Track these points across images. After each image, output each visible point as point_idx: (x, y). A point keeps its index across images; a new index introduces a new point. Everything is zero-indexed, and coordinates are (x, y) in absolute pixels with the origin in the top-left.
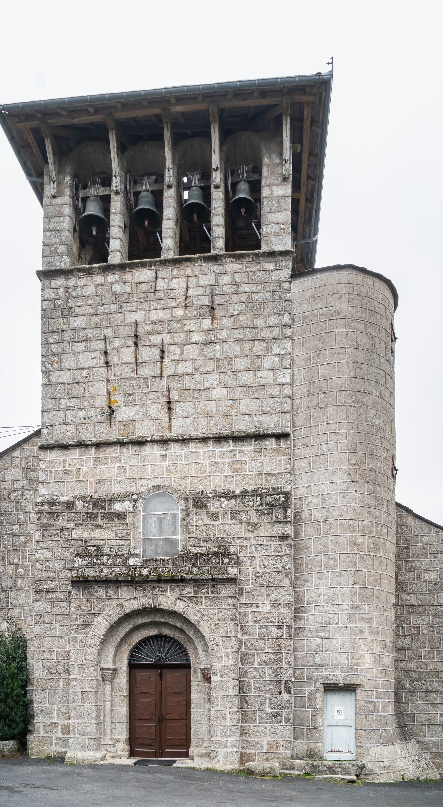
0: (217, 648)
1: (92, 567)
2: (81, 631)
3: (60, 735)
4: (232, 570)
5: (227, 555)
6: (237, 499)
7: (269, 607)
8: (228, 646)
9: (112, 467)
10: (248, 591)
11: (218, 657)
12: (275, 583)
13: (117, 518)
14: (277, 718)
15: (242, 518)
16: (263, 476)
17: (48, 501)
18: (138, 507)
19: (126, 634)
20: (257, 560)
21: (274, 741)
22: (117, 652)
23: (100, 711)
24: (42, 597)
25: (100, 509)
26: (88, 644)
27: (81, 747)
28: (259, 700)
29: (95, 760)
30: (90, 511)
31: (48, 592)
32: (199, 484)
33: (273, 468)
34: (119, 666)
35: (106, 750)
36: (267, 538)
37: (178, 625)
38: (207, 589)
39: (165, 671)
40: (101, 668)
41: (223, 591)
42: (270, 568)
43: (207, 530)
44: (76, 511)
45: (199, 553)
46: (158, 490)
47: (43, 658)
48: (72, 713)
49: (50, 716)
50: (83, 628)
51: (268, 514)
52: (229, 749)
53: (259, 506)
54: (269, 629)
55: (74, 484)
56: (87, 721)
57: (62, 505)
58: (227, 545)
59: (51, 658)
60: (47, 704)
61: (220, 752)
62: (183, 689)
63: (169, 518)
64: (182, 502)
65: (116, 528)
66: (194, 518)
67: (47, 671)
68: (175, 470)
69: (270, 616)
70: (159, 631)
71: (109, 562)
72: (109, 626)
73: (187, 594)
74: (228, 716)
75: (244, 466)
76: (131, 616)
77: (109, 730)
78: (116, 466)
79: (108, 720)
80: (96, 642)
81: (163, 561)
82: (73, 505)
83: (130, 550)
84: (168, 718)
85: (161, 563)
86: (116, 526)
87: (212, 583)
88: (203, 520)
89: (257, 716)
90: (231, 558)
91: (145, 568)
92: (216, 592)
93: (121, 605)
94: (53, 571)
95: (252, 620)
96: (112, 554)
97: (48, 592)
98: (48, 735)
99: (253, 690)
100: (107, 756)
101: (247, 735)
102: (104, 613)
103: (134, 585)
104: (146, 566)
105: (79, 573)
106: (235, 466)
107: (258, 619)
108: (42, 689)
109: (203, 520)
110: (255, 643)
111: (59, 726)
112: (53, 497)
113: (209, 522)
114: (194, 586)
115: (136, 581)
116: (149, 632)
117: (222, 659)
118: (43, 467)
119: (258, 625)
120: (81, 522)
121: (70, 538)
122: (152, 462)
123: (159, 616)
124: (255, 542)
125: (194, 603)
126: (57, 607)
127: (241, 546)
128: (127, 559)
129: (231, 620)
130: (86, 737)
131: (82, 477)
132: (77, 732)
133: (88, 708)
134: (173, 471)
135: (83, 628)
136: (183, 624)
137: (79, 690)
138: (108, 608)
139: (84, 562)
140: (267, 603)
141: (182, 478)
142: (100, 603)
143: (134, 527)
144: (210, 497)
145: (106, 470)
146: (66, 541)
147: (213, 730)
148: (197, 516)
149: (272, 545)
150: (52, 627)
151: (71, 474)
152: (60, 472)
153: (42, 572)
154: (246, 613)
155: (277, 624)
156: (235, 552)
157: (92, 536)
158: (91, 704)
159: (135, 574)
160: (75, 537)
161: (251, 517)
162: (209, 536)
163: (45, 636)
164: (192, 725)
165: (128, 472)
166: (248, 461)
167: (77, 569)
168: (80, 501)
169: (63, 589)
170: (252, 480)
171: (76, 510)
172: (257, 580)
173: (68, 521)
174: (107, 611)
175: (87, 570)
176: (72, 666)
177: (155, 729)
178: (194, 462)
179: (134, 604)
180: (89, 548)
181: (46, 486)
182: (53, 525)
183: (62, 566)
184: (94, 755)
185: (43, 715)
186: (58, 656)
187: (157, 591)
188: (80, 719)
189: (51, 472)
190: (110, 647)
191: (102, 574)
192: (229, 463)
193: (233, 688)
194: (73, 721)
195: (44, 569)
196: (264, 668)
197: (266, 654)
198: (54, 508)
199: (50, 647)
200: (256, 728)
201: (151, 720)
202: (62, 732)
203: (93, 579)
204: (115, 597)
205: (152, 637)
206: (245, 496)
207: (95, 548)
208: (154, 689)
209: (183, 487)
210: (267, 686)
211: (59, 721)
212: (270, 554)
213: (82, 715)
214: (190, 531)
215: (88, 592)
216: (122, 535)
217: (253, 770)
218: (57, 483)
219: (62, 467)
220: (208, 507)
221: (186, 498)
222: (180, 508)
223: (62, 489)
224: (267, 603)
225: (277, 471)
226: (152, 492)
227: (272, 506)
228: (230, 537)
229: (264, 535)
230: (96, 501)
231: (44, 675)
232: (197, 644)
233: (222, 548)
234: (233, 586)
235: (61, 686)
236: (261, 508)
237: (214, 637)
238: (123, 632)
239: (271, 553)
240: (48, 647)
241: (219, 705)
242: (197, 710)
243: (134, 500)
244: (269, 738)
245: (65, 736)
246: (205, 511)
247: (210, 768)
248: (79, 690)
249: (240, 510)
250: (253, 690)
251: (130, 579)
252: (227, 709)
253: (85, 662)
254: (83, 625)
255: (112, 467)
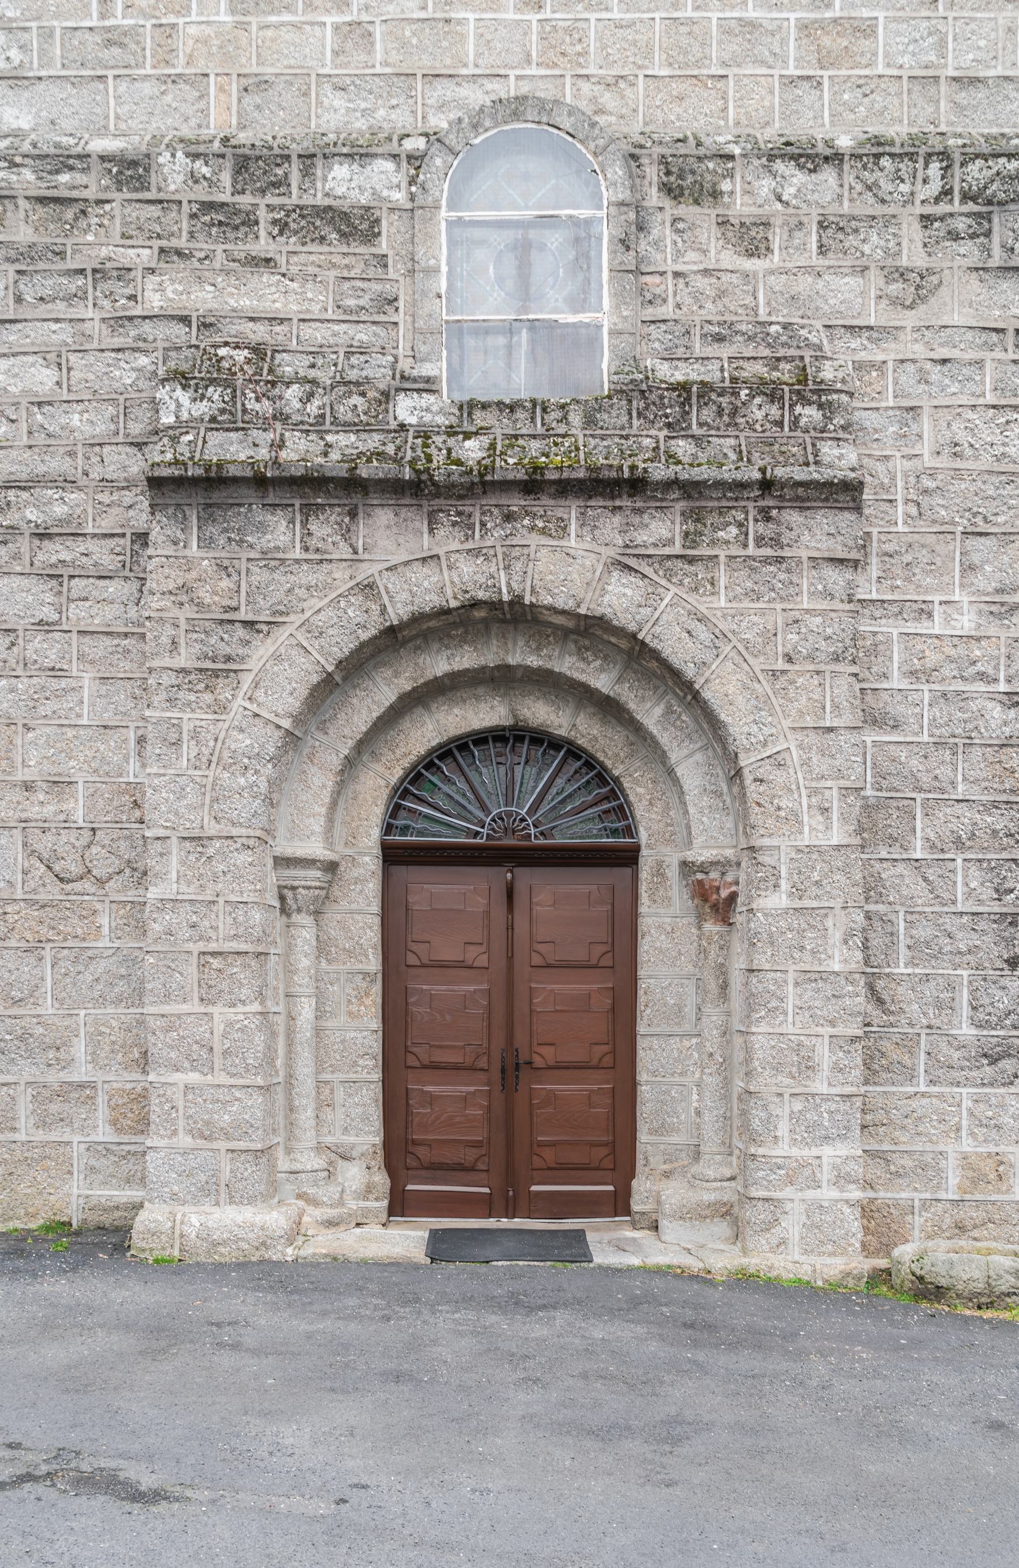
0: (778, 777)
1: (237, 430)
2: (192, 697)
3: (104, 1133)
4: (836, 452)
5: (813, 392)
6: (846, 167)
7: (974, 616)
8: (824, 767)
9: (312, 24)
10: (889, 548)
11: (782, 814)
12: (1000, 519)
13: (339, 231)
14: (1001, 1064)
15: (867, 249)
16: (943, 87)
17: (37, 152)
18: (429, 185)
19: (379, 718)
20: (926, 425)
21: (989, 1155)
22: (339, 793)
23: (274, 1034)
24: (16, 557)
25: (263, 192)
26: (226, 754)
27: (202, 1189)
28: (929, 990)
29: (263, 1244)
30: (225, 197)
31: (43, 536)
32: (680, 111)
33: (980, 54)
34: (349, 851)
35: (299, 1196)
36: (969, 335)
37: (603, 682)
38: (740, 525)
39: (526, 877)
40: (275, 858)
41: (806, 537)
42: (976, 458)
43: (721, 294)
44: (162, 196)
45: (696, 382)
46: (516, 115)
47: (24, 815)
48: (159, 1046)
49: (62, 1055)
50: (201, 686)
51: (973, 236)
52: (828, 1193)
53: (937, 200)
54: (973, 706)
55: (148, 88)
56: (223, 1079)
57: (96, 166)
58: (807, 354)
59: (62, 817)
60: (48, 1008)
61: (788, 1206)
62: (600, 949)
63: (555, 239)
64: (618, 171)
65: (333, 273)
66: (668, 242)
67: (43, 868)
68: (579, 48)
69: (978, 653)
70: (513, 712)
71: (313, 408)
72: (315, 679)
73: (656, 545)
74: (824, 1056)
75: (865, 44)
76: (404, 643)
77: (310, 1113)
78: (329, 20)
79: (306, 1070)
80: (262, 746)
81: (544, 410)
82: (147, 170)
83: (400, 366)
84: (538, 1061)
85: (533, 419)
86: (334, 265)
87: (761, 503)
88: (705, 252)
89: (923, 1056)
90: (830, 403)
91: (467, 436)
92: (776, 542)
93: (368, 588)
94: (62, 450)
95: (904, 669)
96: (325, 377)
97: (43, 536)
98: (54, 1136)
99: (903, 953)
100: (306, 1219)
101: (881, 1130)
102: (296, 619)
103: (425, 502)
104: (474, 430)
105: (183, 449)
106: (826, 41)
107: (929, 664)
108: (23, 944)
109: (705, 252)
110: (915, 763)
111: (101, 1099)
112: (58, 139)
113: (729, 259)
114: (683, 514)
115: (434, 484)
116: (470, 714)
117: (800, 823)
118: (10, 14)
119: (926, 687)
120: (182, 242)
121: (138, 311)
122: (484, 11)
123: (521, 643)
124: (919, 350)
125: (681, 584)
126: (86, 599)
127: (859, 366)
128: (386, 396)
129: (836, 659)
130: (222, 1145)
131: (182, 60)
132: (181, 1123)
133: (230, 1024)
134: (569, 50)
135: (201, 686)
136: (619, 680)
137: (190, 946)
138: (312, 601)
139: (202, 408)
140: (966, 599)
141: (610, 80)
142: (276, 576)
143: (412, 272)
144: (731, 157)
145: (288, 37)
146: (120, 322)
147: (763, 1115)
148: (678, 231)
149: (989, 366)
150: (64, 683)
151: (133, 46)
152: (88, 36)
153: (14, 453)
154: (880, 637)
155: (1003, 687)
156: (843, 381)
157: (232, 302)
158: (240, 1008)
159: (429, 459)
160: (157, 304)
161: (905, 243)
162: (729, 318)
163: (31, 723)
164: (644, 1091)
165: (378, 46)
166: (881, 20)
167: (173, 433)
168: (179, 154)
169: (106, 524)
170: (896, 101)
171: (160, 190)
172: (924, 505)
173: (123, 236)
174: (308, 614)
175: (215, 438)
176: (158, 846)
177: (489, 1107)
178: (657, 15)
179: (426, 584)
180: (222, 352)
181: (26, 94)
182: (61, 254)
183: (102, 428)
184: (258, 1219)
185: (30, 1054)
186: (88, 809)
187: (525, 532)
188: (194, 1069)
189: (47, 34)
190: (314, 769)
191: (283, 455)
192: (804, 27)
193: (846, 942)
194: (163, 1080)
195: (25, 440)
196: (950, 865)
197: (960, 809)
198: (64, 178)
199: (55, 770)
200: (914, 1104)
201: (473, 1069)
202: (114, 1122)
203: (249, 473)
204: (346, 552)
205: (481, 738)
206: (877, 156)
207: (244, 354)
208: (483, 948)
209: (613, 119)
210: (960, 936)
211: (99, 1077)
212: (981, 401)
213: (204, 1055)
214: (649, 296)
215: (225, 530)
216: (362, 302)
217: (943, 1282)
218: (76, 82)
219: (95, 15)
220: (726, 199)
221: (633, 157)
222: (606, 195)
223: (98, 110)
224: (966, 599)
225: (999, 71)
226: (487, 123)
227: (990, 203)
228: (818, 324)
229: (957, 319)
230: (247, 158)
231: (32, 884)
232: (678, 763)
233: (785, 366)
234: (847, 514)
235: (105, 930)
236: (943, 208)
237: (767, 731)
238: (370, 710)
239: (983, 395)
240: (47, 767)
241: (785, 1013)
242: (667, 1030)
243: (410, 157)
244: (967, 1145)
245: (125, 1139)
246: (713, 213)
247: (752, 1270)
248: (190, 946)
249: (856, 212)
250: (903, 953)
251: (407, 474)
252: (820, 1030)
253: (212, 828)
254: (201, 670)
255: (312, 24)
